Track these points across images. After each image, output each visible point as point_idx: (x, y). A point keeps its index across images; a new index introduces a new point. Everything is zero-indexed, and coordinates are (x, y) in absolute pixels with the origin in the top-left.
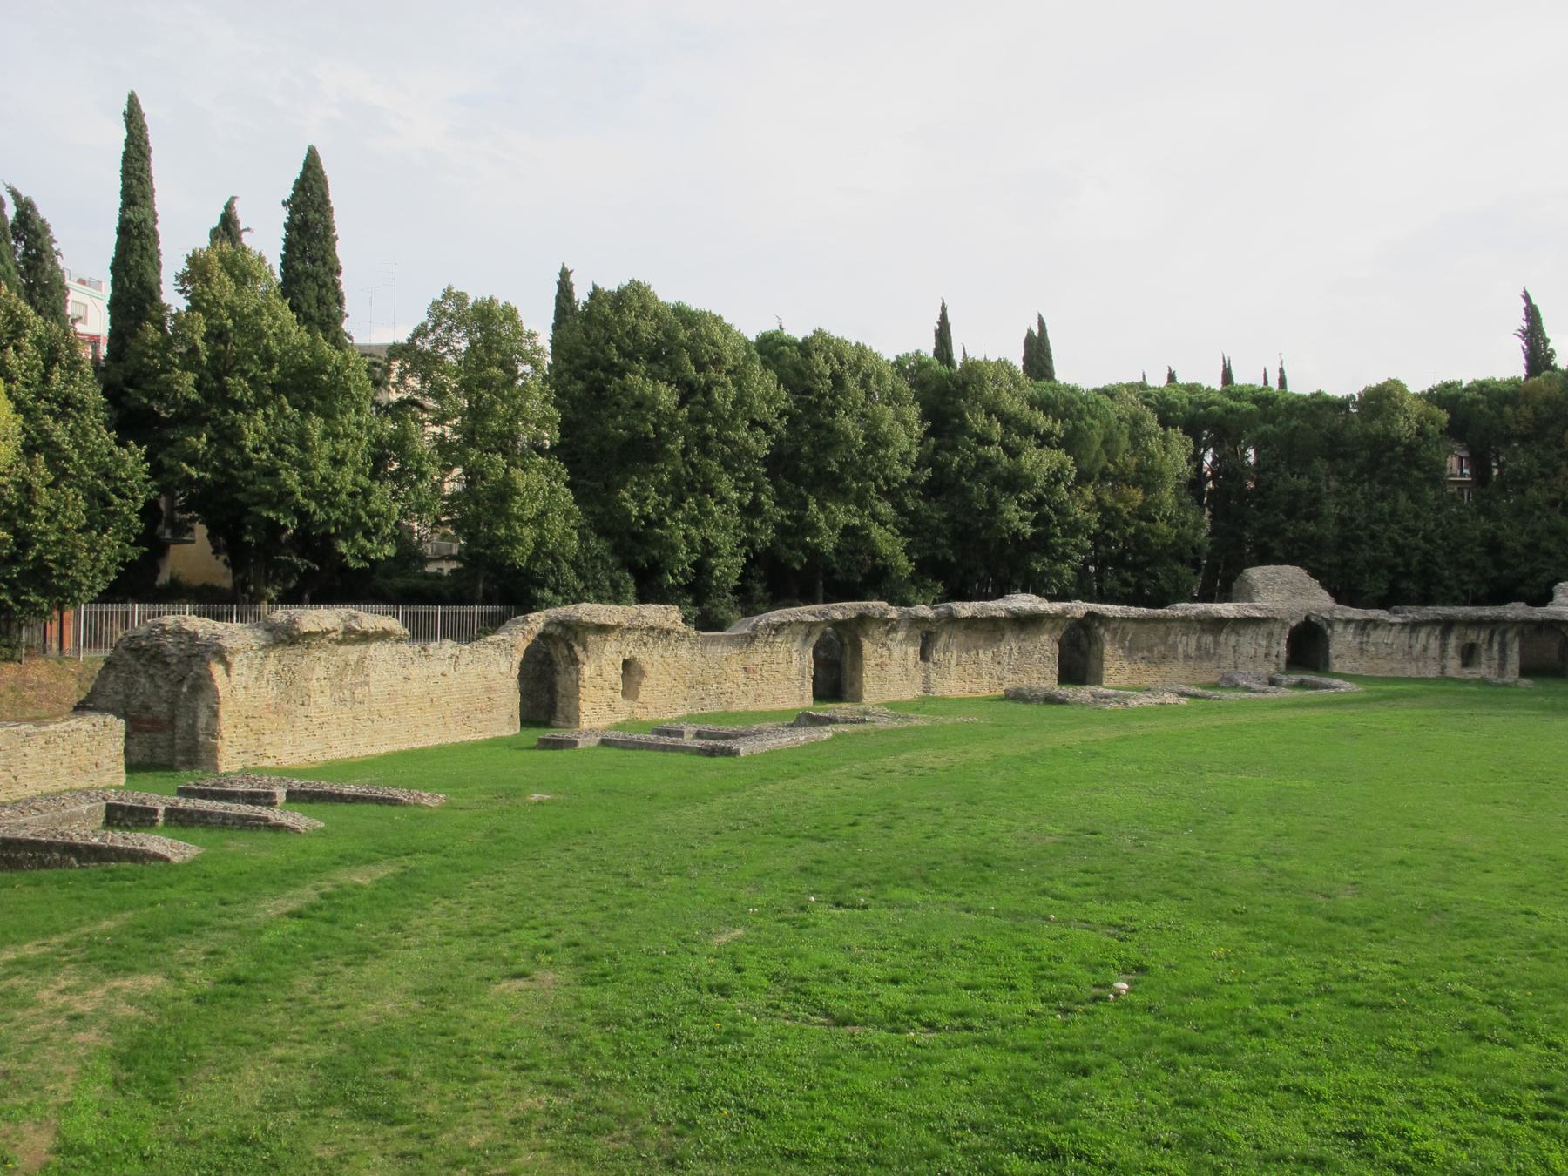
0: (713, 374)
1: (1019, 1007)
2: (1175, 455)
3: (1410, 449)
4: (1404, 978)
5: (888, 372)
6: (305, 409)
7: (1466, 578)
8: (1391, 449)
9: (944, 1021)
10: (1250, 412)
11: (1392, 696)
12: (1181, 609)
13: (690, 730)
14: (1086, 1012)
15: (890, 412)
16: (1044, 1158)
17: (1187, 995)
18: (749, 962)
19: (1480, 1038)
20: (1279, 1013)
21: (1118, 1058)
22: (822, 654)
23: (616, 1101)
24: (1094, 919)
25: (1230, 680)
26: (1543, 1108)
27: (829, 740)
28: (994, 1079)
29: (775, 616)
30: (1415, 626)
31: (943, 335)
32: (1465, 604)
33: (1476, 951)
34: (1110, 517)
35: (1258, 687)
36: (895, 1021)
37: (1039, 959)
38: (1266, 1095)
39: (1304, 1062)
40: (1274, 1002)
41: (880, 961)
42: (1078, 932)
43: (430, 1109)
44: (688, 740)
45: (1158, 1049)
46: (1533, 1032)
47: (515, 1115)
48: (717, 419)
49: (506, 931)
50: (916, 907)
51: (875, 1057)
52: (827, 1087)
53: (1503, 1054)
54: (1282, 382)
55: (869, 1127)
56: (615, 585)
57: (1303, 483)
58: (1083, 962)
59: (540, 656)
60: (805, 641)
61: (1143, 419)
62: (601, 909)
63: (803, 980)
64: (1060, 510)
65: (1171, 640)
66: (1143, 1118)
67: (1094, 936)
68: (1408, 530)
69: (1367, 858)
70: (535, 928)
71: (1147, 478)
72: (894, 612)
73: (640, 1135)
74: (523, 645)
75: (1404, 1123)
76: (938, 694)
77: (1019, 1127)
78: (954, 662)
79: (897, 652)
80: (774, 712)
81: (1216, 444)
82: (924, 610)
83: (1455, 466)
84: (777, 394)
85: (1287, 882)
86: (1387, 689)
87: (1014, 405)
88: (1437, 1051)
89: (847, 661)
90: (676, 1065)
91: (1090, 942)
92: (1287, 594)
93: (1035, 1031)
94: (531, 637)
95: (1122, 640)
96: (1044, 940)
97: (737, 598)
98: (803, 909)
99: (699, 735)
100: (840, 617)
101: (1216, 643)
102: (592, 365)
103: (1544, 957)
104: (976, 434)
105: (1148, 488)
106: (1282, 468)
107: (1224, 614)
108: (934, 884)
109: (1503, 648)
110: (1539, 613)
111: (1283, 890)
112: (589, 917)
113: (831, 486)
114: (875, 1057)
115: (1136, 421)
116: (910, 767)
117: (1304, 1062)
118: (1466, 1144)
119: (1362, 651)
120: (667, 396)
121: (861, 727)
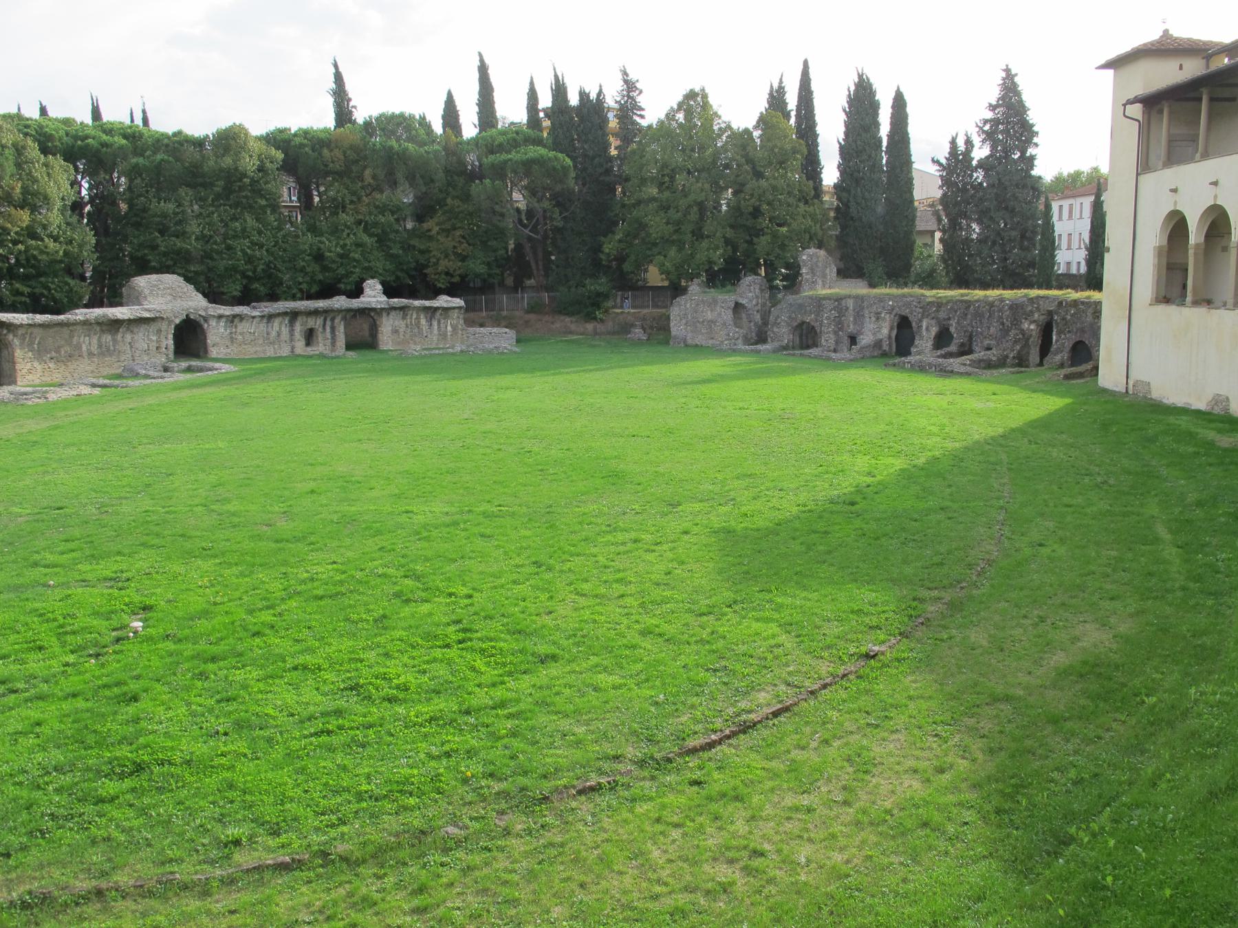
1: (53, 662)
2: (62, 183)
3: (254, 182)
4: (344, 572)
7: (301, 280)
8: (240, 180)
10: (121, 147)
11: (262, 372)
12: (80, 314)
14: (115, 652)
16: (131, 774)
17: (192, 619)
19: (408, 601)
20: (267, 617)
21: (158, 681)
24: (89, 576)
25: (132, 370)
26: (461, 636)
28: (57, 726)
30: (270, 317)
32: (302, 299)
33: (384, 544)
35: (156, 374)
37: (55, 620)
38: (282, 677)
39: (298, 647)
40: (260, 610)
42: (80, 590)
45: (186, 666)
46: (438, 589)
53: (425, 608)
54: (145, 121)
57: (171, 207)
58: (96, 614)
61: (24, 147)
66: (199, 720)
67: (96, 591)
68: (253, 244)
69: (287, 493)
71: (32, 200)
75: (382, 670)
77: (99, 756)
81: (90, 172)
83: (288, 195)
86: (257, 368)
88: (384, 616)
91: (96, 596)
92: (169, 298)
93: (76, 678)
95: (31, 344)
96: (52, 602)
101: (115, 341)
103: (427, 539)
105: (34, 209)
106: (151, 195)
107: (120, 316)
109: (333, 329)
110: (355, 303)
115: (19, 150)
117: (298, 647)
118: (424, 672)
119: (232, 340)
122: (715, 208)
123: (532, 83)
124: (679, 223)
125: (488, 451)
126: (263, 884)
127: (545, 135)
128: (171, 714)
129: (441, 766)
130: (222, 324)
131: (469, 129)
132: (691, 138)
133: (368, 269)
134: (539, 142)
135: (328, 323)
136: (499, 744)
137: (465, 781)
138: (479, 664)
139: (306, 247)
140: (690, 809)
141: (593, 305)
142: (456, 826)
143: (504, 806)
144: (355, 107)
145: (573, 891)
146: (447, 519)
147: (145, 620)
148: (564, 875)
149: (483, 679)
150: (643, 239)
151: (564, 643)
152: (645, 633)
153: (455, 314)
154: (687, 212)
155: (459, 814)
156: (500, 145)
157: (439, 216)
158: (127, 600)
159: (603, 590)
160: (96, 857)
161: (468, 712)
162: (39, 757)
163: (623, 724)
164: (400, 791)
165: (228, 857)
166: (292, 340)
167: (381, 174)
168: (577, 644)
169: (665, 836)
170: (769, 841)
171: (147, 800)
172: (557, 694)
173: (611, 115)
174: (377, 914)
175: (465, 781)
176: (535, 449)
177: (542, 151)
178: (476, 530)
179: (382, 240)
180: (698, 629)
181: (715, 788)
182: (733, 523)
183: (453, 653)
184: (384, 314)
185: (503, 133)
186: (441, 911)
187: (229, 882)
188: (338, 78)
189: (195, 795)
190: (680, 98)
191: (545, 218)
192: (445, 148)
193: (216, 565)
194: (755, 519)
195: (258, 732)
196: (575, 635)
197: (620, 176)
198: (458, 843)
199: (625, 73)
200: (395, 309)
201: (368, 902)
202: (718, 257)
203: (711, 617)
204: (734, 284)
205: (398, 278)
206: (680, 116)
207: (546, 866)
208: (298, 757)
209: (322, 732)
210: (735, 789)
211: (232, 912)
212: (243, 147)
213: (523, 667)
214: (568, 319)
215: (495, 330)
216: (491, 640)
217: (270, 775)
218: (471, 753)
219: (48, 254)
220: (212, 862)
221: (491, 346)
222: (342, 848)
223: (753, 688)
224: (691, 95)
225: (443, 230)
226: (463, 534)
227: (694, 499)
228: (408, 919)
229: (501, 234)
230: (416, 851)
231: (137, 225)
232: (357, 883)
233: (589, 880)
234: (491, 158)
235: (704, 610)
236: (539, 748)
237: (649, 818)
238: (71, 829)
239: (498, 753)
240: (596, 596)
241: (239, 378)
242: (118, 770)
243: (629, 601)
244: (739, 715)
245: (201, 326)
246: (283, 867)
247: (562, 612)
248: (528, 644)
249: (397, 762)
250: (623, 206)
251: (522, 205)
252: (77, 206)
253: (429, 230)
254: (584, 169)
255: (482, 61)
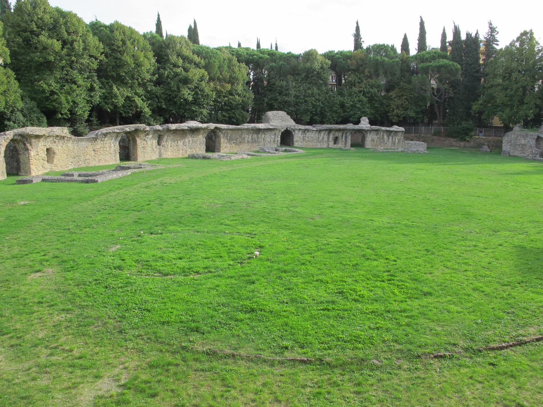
0: (75, 37)
1: (225, 263)
2: (245, 73)
3: (318, 73)
4: (342, 243)
5: (142, 40)
6: (536, 65)
8: (313, 73)
9: (201, 271)
10: (267, 59)
11: (314, 154)
12: (246, 126)
13: (76, 174)
14: (248, 263)
15: (142, 54)
16: (249, 312)
17: (278, 254)
18: (126, 257)
19: (368, 259)
20: (308, 257)
22: (121, 144)
23: (92, 313)
24: (241, 231)
26: (389, 278)
27: (130, 175)
28: (224, 288)
29: (104, 130)
30: (320, 131)
31: (159, 25)
32: (334, 124)
33: (360, 233)
34: (219, 93)
35: (272, 152)
36: (185, 272)
37: (227, 247)
38: (312, 283)
39: (319, 272)
40: (306, 254)
41: (173, 252)
43: (18, 326)
44: (76, 177)
45: (275, 272)
47: (54, 324)
48: (77, 55)
49: (27, 255)
50: (179, 232)
51: (182, 285)
52: (169, 298)
53: (375, 263)
55: (188, 310)
56: (38, 119)
57: (284, 83)
58: (242, 246)
59: (11, 148)
60: (116, 139)
61: (232, 59)
62: (63, 243)
63: (147, 261)
64: (202, 91)
65: (243, 136)
66: (277, 295)
67: (243, 237)
68: (317, 100)
69: (321, 206)
70: (38, 253)
71: (232, 80)
72: (148, 128)
73: (105, 323)
74: (5, 144)
75: (354, 287)
76: (164, 157)
78: (169, 146)
79: (149, 142)
80: (106, 166)
81: (254, 69)
82: (158, 127)
83: (331, 79)
84: (99, 46)
85: (299, 215)
86: (313, 152)
87: (187, 52)
88: (357, 264)
89: (131, 147)
90: (111, 297)
91: (242, 239)
94: (8, 141)
95: (227, 137)
96: (226, 239)
97: (87, 124)
98: (139, 236)
99: (80, 175)
100: (129, 130)
101: (258, 137)
102: (25, 31)
103: (379, 233)
104: (173, 64)
105: (233, 84)
106: (277, 78)
107: (261, 127)
108: (183, 224)
110: (356, 127)
111: (298, 218)
112: (59, 246)
113: (121, 81)
114: (182, 285)
115: (230, 61)
116: (163, 184)
117: (319, 272)
118: (372, 291)
120: (57, 45)
121: (141, 170)
122: (531, 89)
123: (444, 30)
124: (512, 96)
125: (410, 197)
126: (295, 367)
127: (448, 54)
128: (266, 291)
129: (374, 333)
130: (300, 133)
131: (413, 51)
132: (523, 55)
133: (364, 112)
134: (445, 57)
135: (344, 135)
136: (401, 328)
137: (384, 341)
138: (396, 291)
139: (338, 101)
140: (487, 376)
141: (464, 134)
142: (378, 360)
143: (400, 356)
144: (363, 42)
145: (426, 401)
146: (388, 225)
147: (260, 252)
148: (423, 392)
149: (397, 298)
150: (493, 104)
151: (436, 288)
152: (474, 289)
153: (400, 134)
154: (517, 91)
155: (379, 355)
156: (427, 59)
157: (397, 90)
158: (254, 242)
159: (456, 267)
160: (233, 342)
161: (388, 312)
162: (217, 299)
163: (460, 330)
164: (355, 340)
165: (282, 353)
166: (328, 141)
167: (372, 71)
168: (442, 290)
169: (473, 386)
170: (527, 401)
171: (254, 324)
172: (430, 310)
173: (481, 44)
174: (339, 390)
175: (384, 341)
176: (431, 198)
177: (446, 61)
178: (401, 232)
179: (371, 99)
180: (501, 292)
181: (501, 369)
182: (526, 244)
183: (385, 285)
184: (369, 133)
185: (428, 53)
186: (366, 395)
187: (282, 363)
188: (358, 29)
189: (273, 325)
190: (518, 35)
191: (445, 92)
192: (402, 60)
193: (290, 233)
194: (537, 243)
195: (299, 304)
196: (441, 285)
197: (484, 74)
198: (378, 368)
199: (491, 24)
200: (373, 130)
201: (335, 384)
202: (531, 114)
203: (509, 287)
204: (538, 127)
205: (375, 117)
206: (517, 44)
207: (415, 386)
208: (315, 318)
209: (326, 309)
210: (512, 371)
211: (282, 375)
212: (315, 58)
213: (416, 296)
214: (452, 140)
215: (417, 142)
216: (403, 282)
217: (303, 323)
218: (388, 330)
219: (236, 101)
220: (276, 354)
221: (415, 150)
222: (328, 359)
223: (527, 325)
224: (525, 33)
225: (398, 96)
226: (395, 233)
227: (506, 229)
228: (352, 395)
229: (424, 99)
230: (359, 367)
231: (270, 91)
232: (333, 375)
233: (434, 397)
234: (422, 65)
235: (506, 283)
236: (418, 334)
237: (467, 376)
238: (226, 329)
239: (399, 332)
240: (453, 269)
241: (306, 156)
242: (244, 310)
243: (469, 273)
244: (518, 336)
245: (291, 133)
246: (303, 362)
247: (436, 274)
248: (419, 286)
249: (356, 328)
250: (484, 88)
251: (435, 86)
252: (248, 83)
253: (391, 96)
254: (466, 70)
255: (422, 20)
